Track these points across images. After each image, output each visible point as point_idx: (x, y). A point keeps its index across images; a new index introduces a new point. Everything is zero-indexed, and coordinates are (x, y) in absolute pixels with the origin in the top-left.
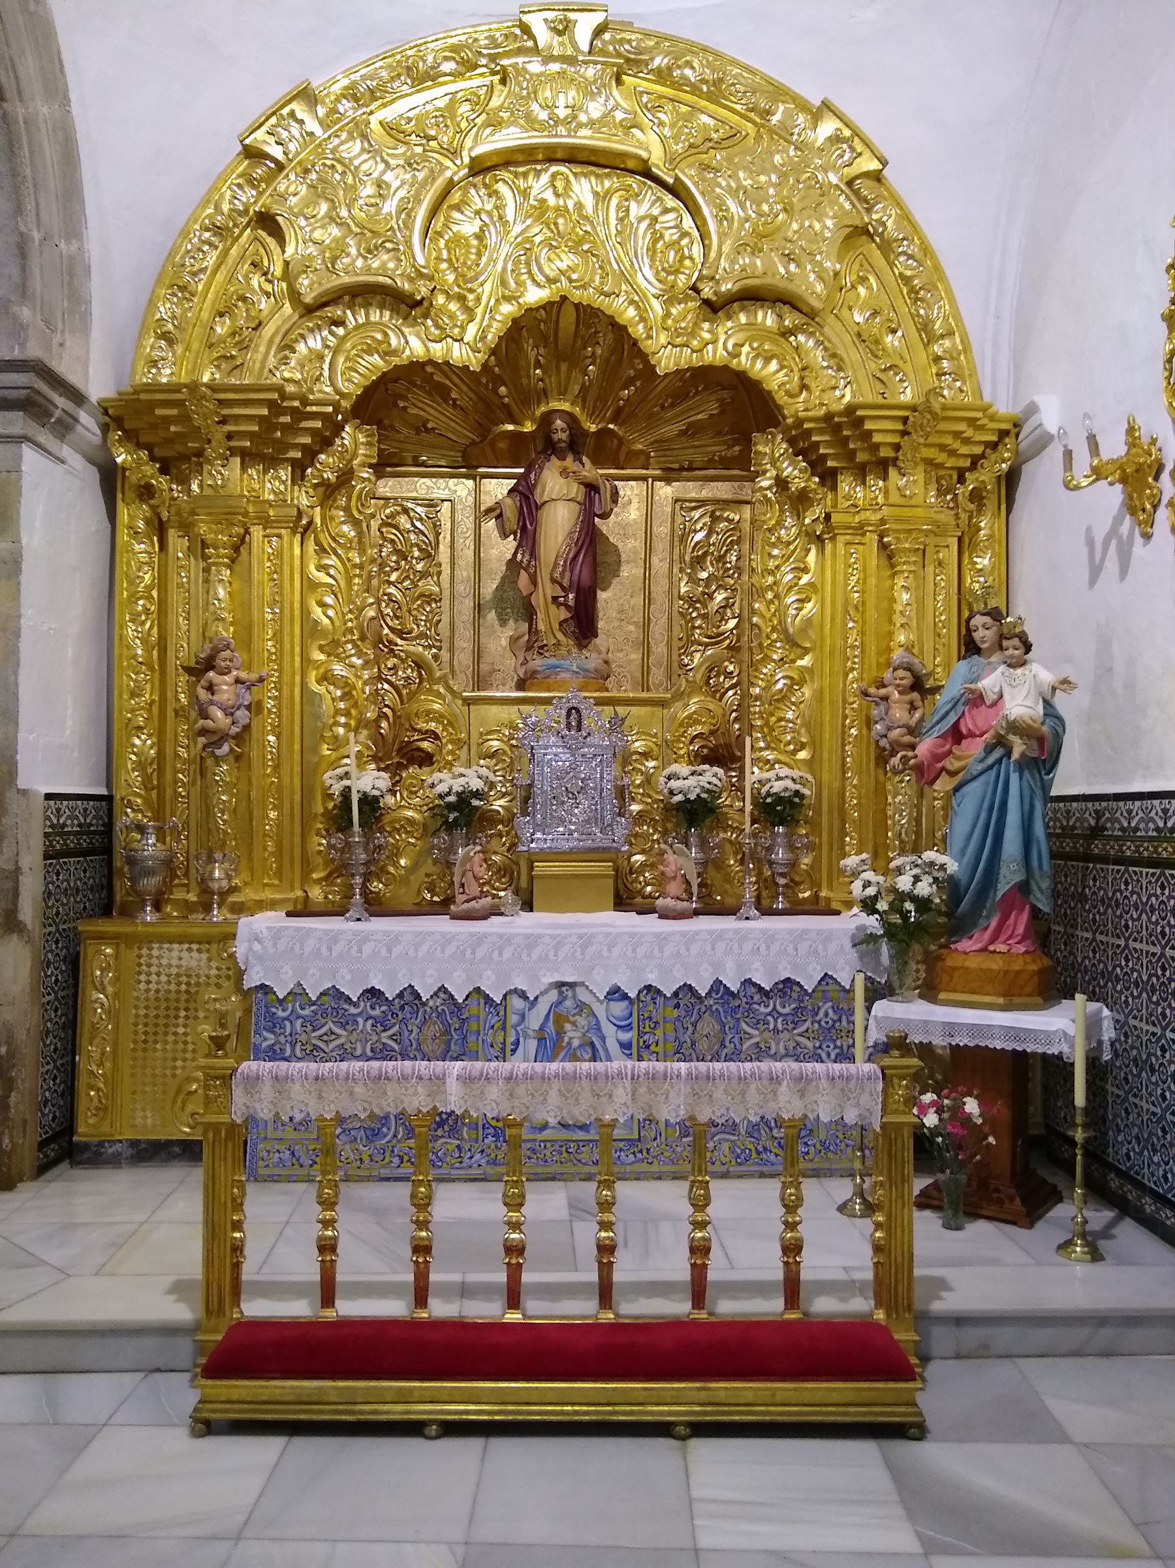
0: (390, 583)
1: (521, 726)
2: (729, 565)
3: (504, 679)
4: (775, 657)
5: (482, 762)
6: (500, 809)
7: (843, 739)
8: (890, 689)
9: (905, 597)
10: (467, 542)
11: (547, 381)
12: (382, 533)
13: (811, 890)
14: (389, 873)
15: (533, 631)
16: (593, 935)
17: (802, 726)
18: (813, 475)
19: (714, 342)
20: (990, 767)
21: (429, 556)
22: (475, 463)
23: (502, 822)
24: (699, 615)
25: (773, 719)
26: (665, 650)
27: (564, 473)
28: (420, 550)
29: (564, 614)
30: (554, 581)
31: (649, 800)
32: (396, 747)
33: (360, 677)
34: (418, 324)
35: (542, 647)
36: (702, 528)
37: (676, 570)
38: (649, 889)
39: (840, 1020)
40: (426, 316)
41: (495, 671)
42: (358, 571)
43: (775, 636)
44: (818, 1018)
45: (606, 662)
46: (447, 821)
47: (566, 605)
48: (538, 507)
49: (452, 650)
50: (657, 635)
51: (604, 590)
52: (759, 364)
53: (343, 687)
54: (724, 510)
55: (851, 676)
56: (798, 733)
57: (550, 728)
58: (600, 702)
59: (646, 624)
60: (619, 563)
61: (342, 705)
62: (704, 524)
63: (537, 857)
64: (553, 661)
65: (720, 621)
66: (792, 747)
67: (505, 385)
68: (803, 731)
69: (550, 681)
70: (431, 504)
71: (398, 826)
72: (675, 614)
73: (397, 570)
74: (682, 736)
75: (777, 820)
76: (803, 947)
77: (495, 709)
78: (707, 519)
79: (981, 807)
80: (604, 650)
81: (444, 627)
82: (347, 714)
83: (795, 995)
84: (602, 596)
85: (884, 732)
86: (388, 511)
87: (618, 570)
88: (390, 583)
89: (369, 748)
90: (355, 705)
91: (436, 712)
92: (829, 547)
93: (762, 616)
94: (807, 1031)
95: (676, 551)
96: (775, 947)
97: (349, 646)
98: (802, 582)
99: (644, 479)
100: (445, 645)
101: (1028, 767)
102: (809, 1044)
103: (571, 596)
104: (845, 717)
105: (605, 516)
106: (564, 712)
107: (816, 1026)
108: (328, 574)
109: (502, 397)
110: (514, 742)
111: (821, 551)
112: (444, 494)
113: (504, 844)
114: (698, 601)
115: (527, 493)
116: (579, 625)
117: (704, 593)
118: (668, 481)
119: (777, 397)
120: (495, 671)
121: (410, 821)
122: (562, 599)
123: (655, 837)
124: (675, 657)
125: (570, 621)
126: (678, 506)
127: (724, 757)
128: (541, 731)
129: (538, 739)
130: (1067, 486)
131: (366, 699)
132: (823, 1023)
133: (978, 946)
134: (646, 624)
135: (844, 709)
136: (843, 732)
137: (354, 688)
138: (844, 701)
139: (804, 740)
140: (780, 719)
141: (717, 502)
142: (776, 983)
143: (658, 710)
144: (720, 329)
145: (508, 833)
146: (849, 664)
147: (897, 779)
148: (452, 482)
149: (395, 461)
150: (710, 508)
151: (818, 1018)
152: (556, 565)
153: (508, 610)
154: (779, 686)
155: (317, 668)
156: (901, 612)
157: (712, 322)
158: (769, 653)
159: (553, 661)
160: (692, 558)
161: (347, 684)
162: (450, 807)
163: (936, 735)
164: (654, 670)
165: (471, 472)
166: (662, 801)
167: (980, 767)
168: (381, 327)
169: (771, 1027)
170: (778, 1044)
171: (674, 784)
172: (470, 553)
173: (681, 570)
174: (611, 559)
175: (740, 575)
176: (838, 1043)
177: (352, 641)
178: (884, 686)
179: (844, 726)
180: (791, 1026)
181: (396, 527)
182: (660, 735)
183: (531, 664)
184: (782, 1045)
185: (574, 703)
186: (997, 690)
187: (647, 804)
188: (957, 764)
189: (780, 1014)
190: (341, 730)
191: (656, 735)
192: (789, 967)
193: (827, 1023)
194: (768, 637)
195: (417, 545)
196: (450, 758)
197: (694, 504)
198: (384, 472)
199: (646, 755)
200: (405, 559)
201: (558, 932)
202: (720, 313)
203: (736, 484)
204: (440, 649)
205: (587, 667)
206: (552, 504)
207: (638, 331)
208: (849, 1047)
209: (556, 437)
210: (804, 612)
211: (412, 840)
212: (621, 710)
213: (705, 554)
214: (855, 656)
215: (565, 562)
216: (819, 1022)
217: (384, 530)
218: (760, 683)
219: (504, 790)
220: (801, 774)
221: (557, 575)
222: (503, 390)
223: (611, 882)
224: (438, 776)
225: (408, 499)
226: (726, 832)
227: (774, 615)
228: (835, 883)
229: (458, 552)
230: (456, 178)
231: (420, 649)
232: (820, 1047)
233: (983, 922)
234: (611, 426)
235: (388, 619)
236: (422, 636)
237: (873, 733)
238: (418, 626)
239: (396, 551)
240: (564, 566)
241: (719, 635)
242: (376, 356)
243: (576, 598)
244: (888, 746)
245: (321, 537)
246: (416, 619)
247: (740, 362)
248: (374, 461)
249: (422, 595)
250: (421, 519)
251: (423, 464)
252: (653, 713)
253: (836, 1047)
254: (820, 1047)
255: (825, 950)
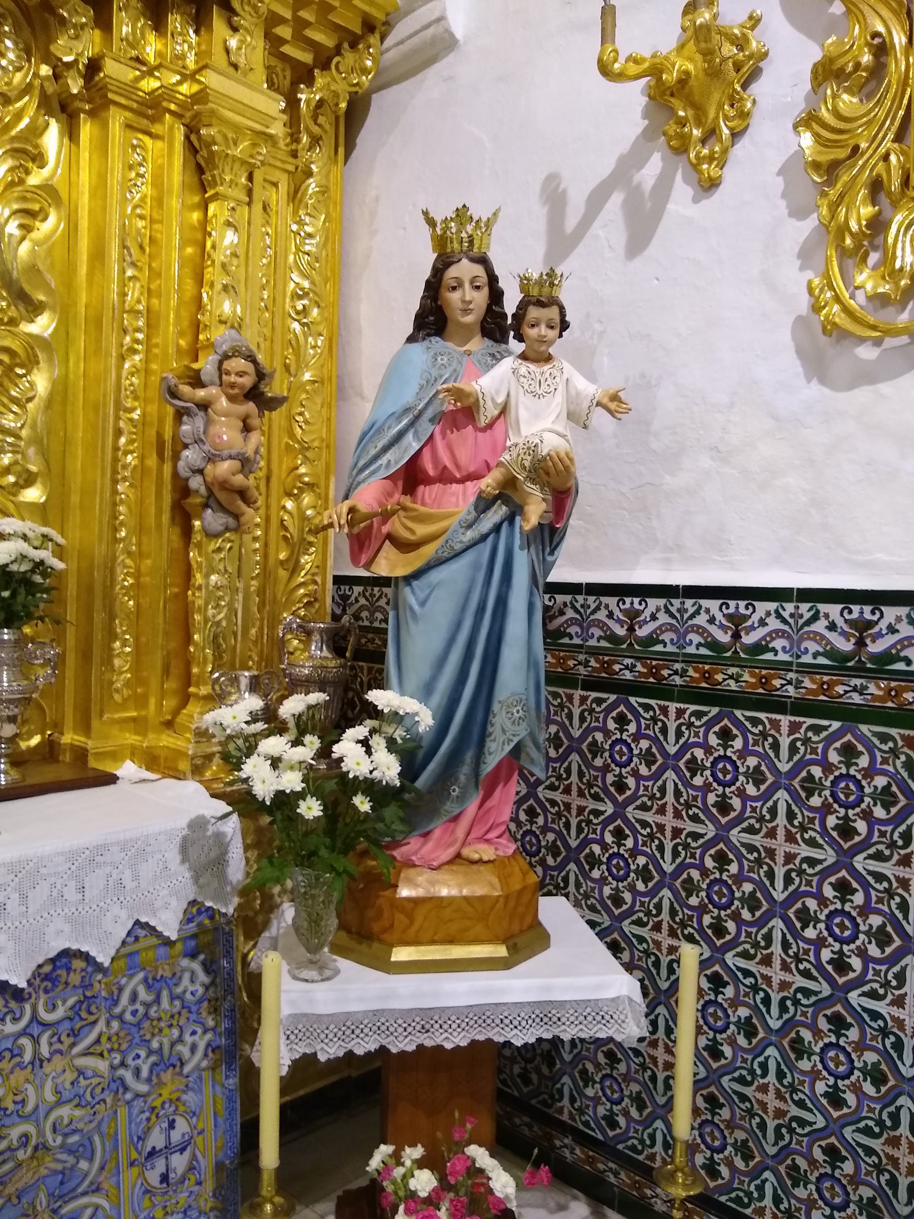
7: (115, 472)
8: (214, 390)
9: (230, 237)
13: (43, 733)
20: (484, 538)
39: (158, 1000)
44: (117, 1010)
55: (127, 365)
66: (11, 479)
68: (31, 451)
76: (95, 882)
79: (464, 608)
83: (75, 979)
85: (199, 464)
92: (86, 129)
94: (98, 1041)
96: (39, 896)
101: (535, 542)
102: (102, 1066)
104: (119, 433)
107: (115, 1024)
111: (71, 133)
130: (605, 70)
132: (128, 1017)
133: (450, 853)
135: (117, 418)
136: (116, 460)
138: (118, 405)
139: (33, 468)
142: (40, 966)
146: (128, 339)
147: (213, 545)
151: (117, 1010)
156: (224, 266)
163: (384, 473)
167: (470, 535)
169: (28, 1057)
170: (40, 1088)
176: (155, 1045)
178: (202, 385)
179: (116, 449)
180: (67, 1041)
184: (49, 1085)
186: (501, 399)
188: (422, 530)
189: (45, 1025)
192: (67, 928)
193: (134, 1013)
208: (173, 1045)
214: (138, 330)
216: (120, 1017)
220: (45, 530)
228: (95, 723)
232: (123, 1064)
233: (451, 808)
237: (181, 464)
244: (203, 490)
253: (150, 1053)
254: (123, 1064)
255: (136, 877)
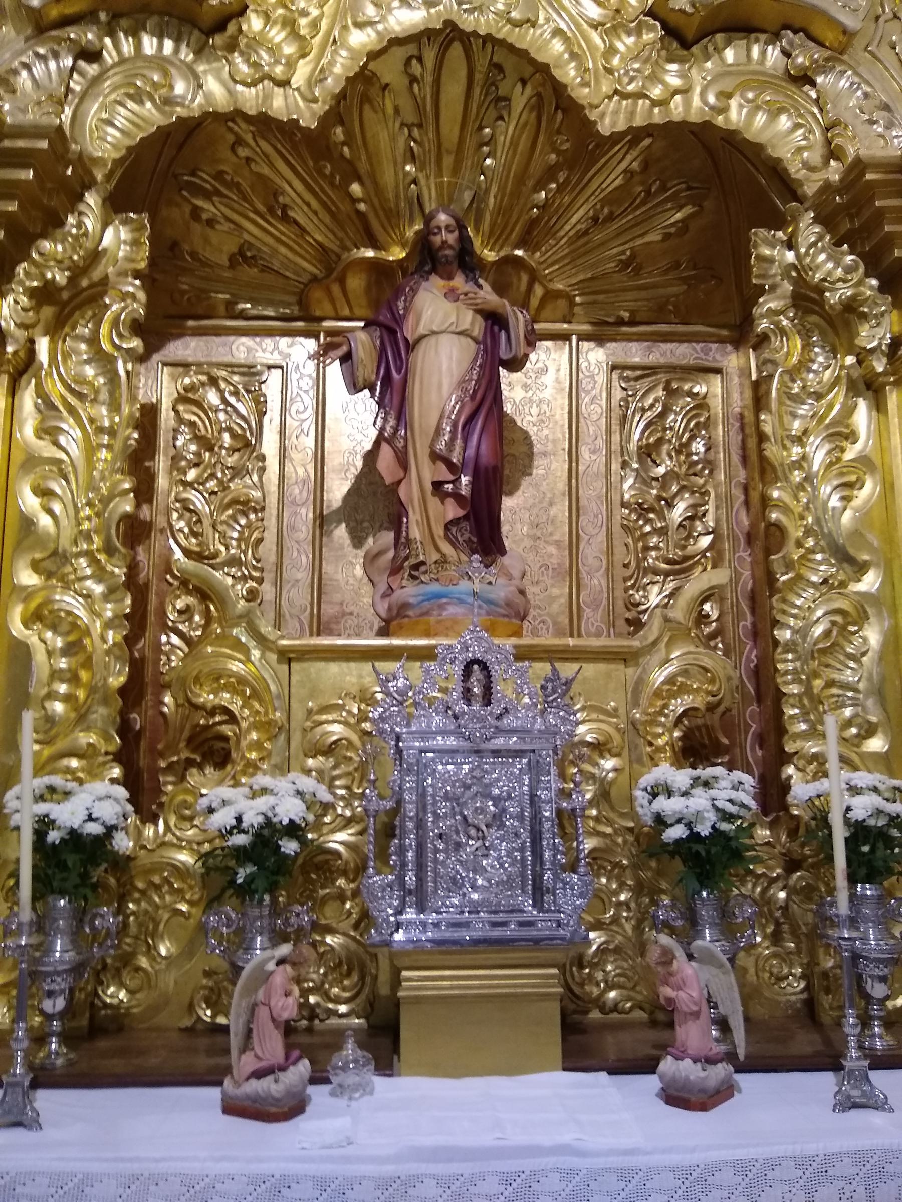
0: (186, 484)
1: (379, 696)
2: (695, 458)
3: (358, 626)
4: (814, 579)
5: (310, 762)
6: (341, 848)
10: (305, 426)
11: (423, 182)
12: (177, 412)
14: (138, 969)
15: (402, 542)
16: (536, 1176)
17: (867, 695)
18: (867, 275)
19: (684, 91)
21: (247, 444)
22: (318, 313)
23: (344, 873)
24: (655, 531)
25: (818, 683)
26: (604, 583)
27: (451, 295)
28: (234, 435)
29: (452, 511)
30: (435, 457)
31: (609, 830)
32: (186, 734)
33: (99, 615)
34: (218, 59)
35: (416, 567)
36: (652, 406)
37: (615, 466)
38: (612, 994)
40: (232, 46)
41: (344, 614)
42: (106, 439)
43: (810, 543)
45: (522, 592)
46: (232, 882)
47: (457, 497)
48: (411, 347)
49: (279, 582)
50: (591, 561)
51: (510, 493)
52: (760, 119)
53: (68, 633)
54: (683, 380)
56: (864, 708)
57: (432, 701)
58: (523, 654)
59: (574, 544)
60: (530, 455)
61: (63, 663)
62: (656, 400)
63: (407, 962)
64: (435, 588)
65: (687, 538)
66: (854, 731)
67: (362, 184)
68: (870, 703)
69: (432, 619)
70: (250, 371)
71: (157, 880)
72: (617, 529)
73: (197, 465)
74: (661, 713)
75: (863, 872)
77: (334, 668)
78: (660, 392)
80: (516, 574)
81: (268, 549)
82: (73, 678)
84: (508, 503)
86: (187, 381)
87: (530, 466)
88: (186, 484)
89: (108, 738)
90: (88, 663)
91: (232, 674)
93: (785, 509)
95: (616, 438)
97: (83, 562)
98: (849, 456)
99: (565, 337)
100: (269, 577)
103: (465, 480)
105: (516, 364)
106: (457, 669)
108: (56, 444)
109: (354, 201)
110: (367, 726)
111: (879, 406)
112: (275, 358)
113: (349, 913)
114: (651, 510)
115: (393, 325)
116: (478, 529)
117: (659, 498)
118: (599, 339)
119: (792, 170)
120: (344, 614)
121: (180, 871)
122: (449, 487)
123: (623, 897)
124: (619, 593)
125: (465, 525)
126: (615, 375)
127: (704, 746)
128: (416, 704)
129: (409, 719)
131: (108, 652)
134: (574, 544)
137: (87, 632)
139: (874, 719)
140: (831, 683)
141: (671, 368)
143: (618, 670)
144: (694, 71)
145: (356, 894)
148: (284, 341)
149: (200, 311)
150: (663, 377)
152: (439, 431)
153: (366, 524)
154: (818, 630)
155: (26, 600)
157: (681, 61)
158: (803, 571)
159: (435, 588)
160: (640, 448)
161: (74, 626)
162: (241, 855)
164: (587, 612)
165: (314, 326)
166: (631, 830)
168: (160, 62)
171: (663, 804)
172: (309, 442)
173: (625, 465)
174: (519, 449)
175: (711, 472)
177: (88, 554)
181: (198, 404)
182: (622, 711)
183: (400, 595)
185: (476, 651)
187: (604, 835)
190: (59, 707)
191: (614, 713)
194: (799, 544)
195: (229, 429)
196: (253, 755)
197: (639, 373)
198: (185, 327)
199: (600, 748)
200: (211, 449)
201: (454, 1168)
202: (695, 49)
203: (698, 346)
204: (260, 581)
205: (492, 596)
206: (433, 340)
207: (569, 74)
209: (437, 240)
210: (856, 503)
211: (184, 907)
212: (567, 669)
213: (660, 441)
215: (455, 426)
217: (181, 408)
218: (792, 622)
219: (348, 813)
221: (441, 446)
222: (356, 188)
223: (555, 1009)
224: (225, 792)
225: (220, 365)
226: (743, 882)
227: (807, 508)
229: (291, 441)
230: (362, 324)
231: (229, 581)
234: (519, 253)
235: (181, 537)
236: (233, 562)
238: (227, 549)
239: (198, 438)
240: (453, 433)
241: (686, 559)
242: (149, 105)
243: (473, 484)
245: (48, 386)
246: (223, 536)
247: (727, 119)
248: (142, 265)
249: (235, 502)
250: (236, 393)
251: (242, 315)
252: (608, 675)
